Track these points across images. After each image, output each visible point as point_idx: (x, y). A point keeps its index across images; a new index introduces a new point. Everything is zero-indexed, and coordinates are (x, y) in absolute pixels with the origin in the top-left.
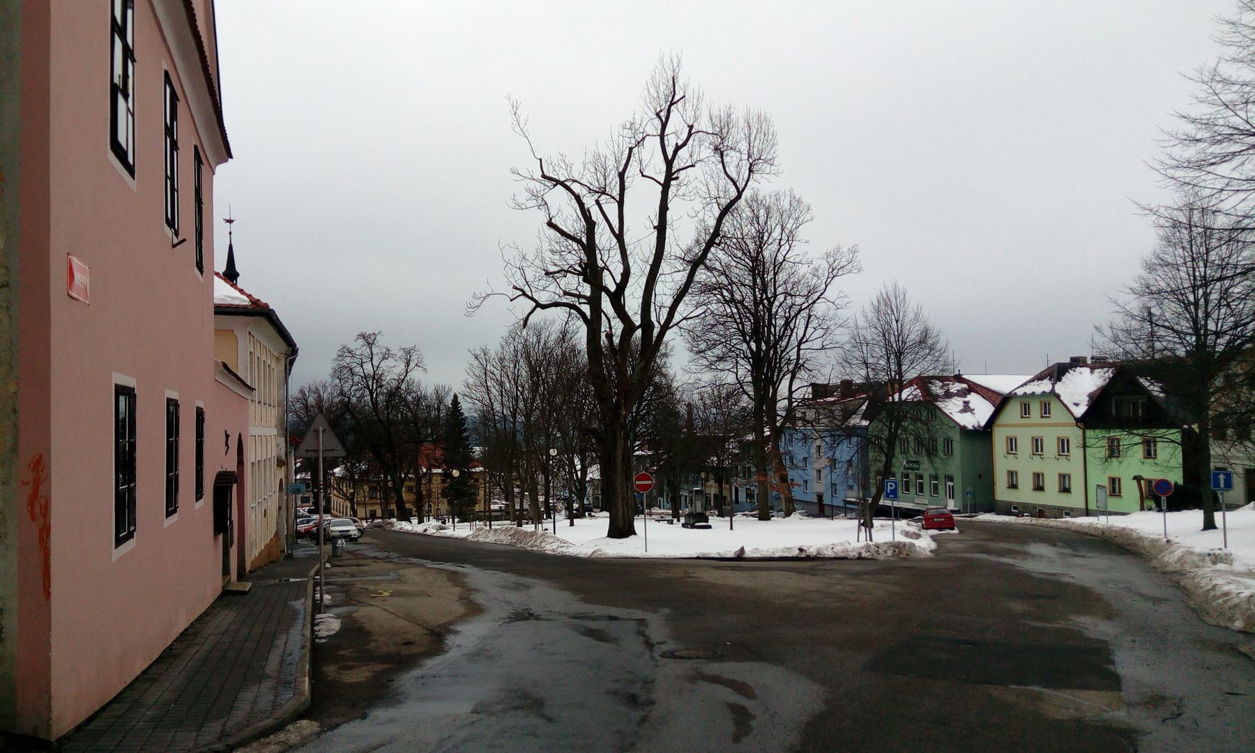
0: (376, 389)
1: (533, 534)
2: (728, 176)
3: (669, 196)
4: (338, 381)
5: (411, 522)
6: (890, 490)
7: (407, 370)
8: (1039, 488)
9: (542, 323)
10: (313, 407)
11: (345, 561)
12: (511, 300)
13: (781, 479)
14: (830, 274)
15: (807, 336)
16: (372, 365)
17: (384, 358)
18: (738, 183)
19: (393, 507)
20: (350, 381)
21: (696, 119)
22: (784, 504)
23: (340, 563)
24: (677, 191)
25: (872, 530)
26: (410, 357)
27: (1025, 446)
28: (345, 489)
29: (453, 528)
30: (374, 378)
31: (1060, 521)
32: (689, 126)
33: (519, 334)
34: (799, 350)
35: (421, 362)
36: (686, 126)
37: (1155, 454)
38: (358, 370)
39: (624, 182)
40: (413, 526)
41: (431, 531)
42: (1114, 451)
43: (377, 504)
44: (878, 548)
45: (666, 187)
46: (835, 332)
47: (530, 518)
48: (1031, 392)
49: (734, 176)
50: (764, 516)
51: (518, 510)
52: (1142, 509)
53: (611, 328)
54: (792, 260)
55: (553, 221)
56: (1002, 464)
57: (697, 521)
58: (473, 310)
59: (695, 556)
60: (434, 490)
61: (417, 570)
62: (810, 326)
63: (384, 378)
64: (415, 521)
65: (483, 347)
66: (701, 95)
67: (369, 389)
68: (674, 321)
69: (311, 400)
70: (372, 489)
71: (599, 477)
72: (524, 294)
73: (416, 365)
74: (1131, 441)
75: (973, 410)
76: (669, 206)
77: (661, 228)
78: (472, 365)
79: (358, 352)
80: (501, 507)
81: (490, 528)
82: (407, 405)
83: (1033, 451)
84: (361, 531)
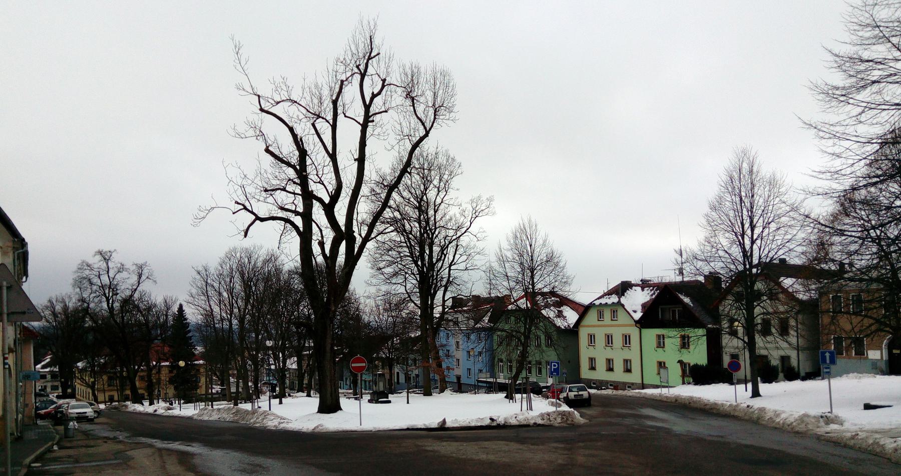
0: (112, 296)
1: (254, 412)
2: (418, 118)
3: (367, 135)
4: (78, 289)
5: (143, 405)
6: (554, 369)
7: (139, 282)
8: (610, 369)
9: (252, 248)
10: (60, 313)
11: (76, 442)
12: (234, 213)
13: (437, 365)
14: (474, 215)
15: (455, 261)
16: (109, 276)
17: (119, 271)
18: (425, 124)
19: (128, 392)
20: (89, 289)
21: (388, 73)
22: (439, 384)
23: (68, 445)
24: (373, 132)
25: (354, 399)
26: (142, 271)
27: (600, 340)
28: (87, 378)
29: (179, 408)
30: (110, 288)
31: (635, 392)
32: (382, 80)
33: (234, 255)
34: (450, 270)
35: (151, 275)
36: (380, 79)
37: (689, 346)
38: (96, 280)
39: (337, 109)
40: (145, 408)
41: (161, 412)
42: (660, 343)
43: (114, 390)
44: (549, 416)
45: (364, 127)
46: (475, 258)
47: (242, 399)
48: (605, 303)
49: (424, 119)
50: (428, 393)
51: (233, 393)
52: (684, 383)
53: (322, 237)
54: (447, 202)
55: (270, 148)
56: (585, 353)
57: (379, 397)
58: (199, 220)
59: (406, 427)
60: (162, 378)
61: (149, 451)
62: (457, 252)
63: (119, 288)
64: (146, 403)
65: (204, 265)
66: (391, 56)
67: (105, 296)
68: (373, 236)
69: (59, 308)
70: (110, 379)
71: (297, 368)
72: (245, 208)
73: (148, 278)
74: (673, 337)
75: (566, 317)
76: (367, 144)
77: (361, 160)
78: (195, 279)
79: (96, 266)
80: (217, 391)
81: (212, 407)
82: (139, 310)
83: (606, 344)
84: (99, 413)
